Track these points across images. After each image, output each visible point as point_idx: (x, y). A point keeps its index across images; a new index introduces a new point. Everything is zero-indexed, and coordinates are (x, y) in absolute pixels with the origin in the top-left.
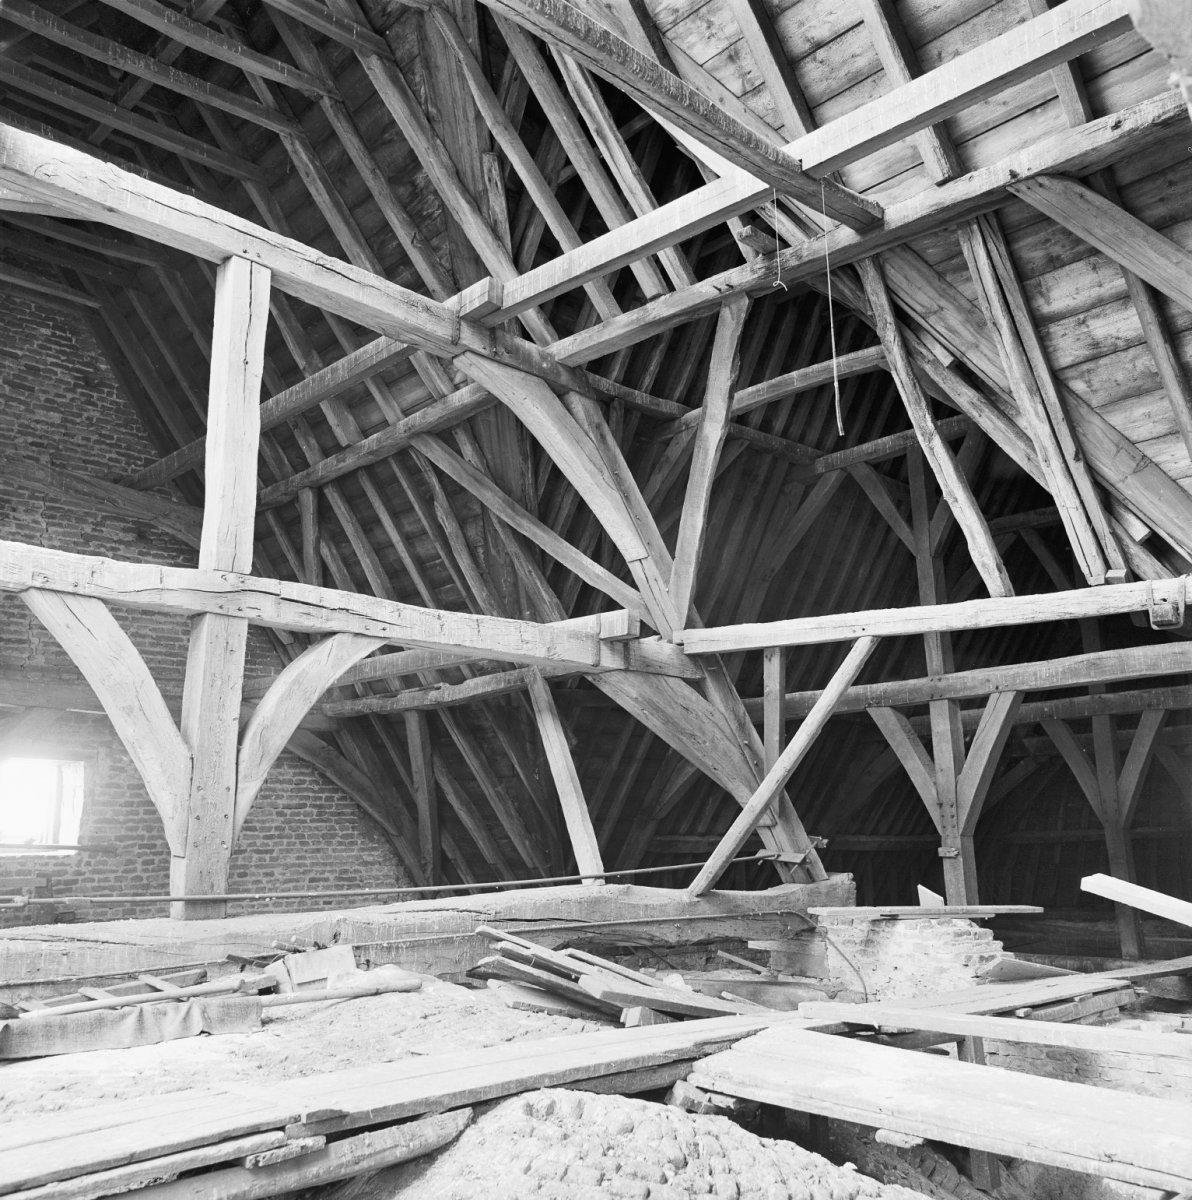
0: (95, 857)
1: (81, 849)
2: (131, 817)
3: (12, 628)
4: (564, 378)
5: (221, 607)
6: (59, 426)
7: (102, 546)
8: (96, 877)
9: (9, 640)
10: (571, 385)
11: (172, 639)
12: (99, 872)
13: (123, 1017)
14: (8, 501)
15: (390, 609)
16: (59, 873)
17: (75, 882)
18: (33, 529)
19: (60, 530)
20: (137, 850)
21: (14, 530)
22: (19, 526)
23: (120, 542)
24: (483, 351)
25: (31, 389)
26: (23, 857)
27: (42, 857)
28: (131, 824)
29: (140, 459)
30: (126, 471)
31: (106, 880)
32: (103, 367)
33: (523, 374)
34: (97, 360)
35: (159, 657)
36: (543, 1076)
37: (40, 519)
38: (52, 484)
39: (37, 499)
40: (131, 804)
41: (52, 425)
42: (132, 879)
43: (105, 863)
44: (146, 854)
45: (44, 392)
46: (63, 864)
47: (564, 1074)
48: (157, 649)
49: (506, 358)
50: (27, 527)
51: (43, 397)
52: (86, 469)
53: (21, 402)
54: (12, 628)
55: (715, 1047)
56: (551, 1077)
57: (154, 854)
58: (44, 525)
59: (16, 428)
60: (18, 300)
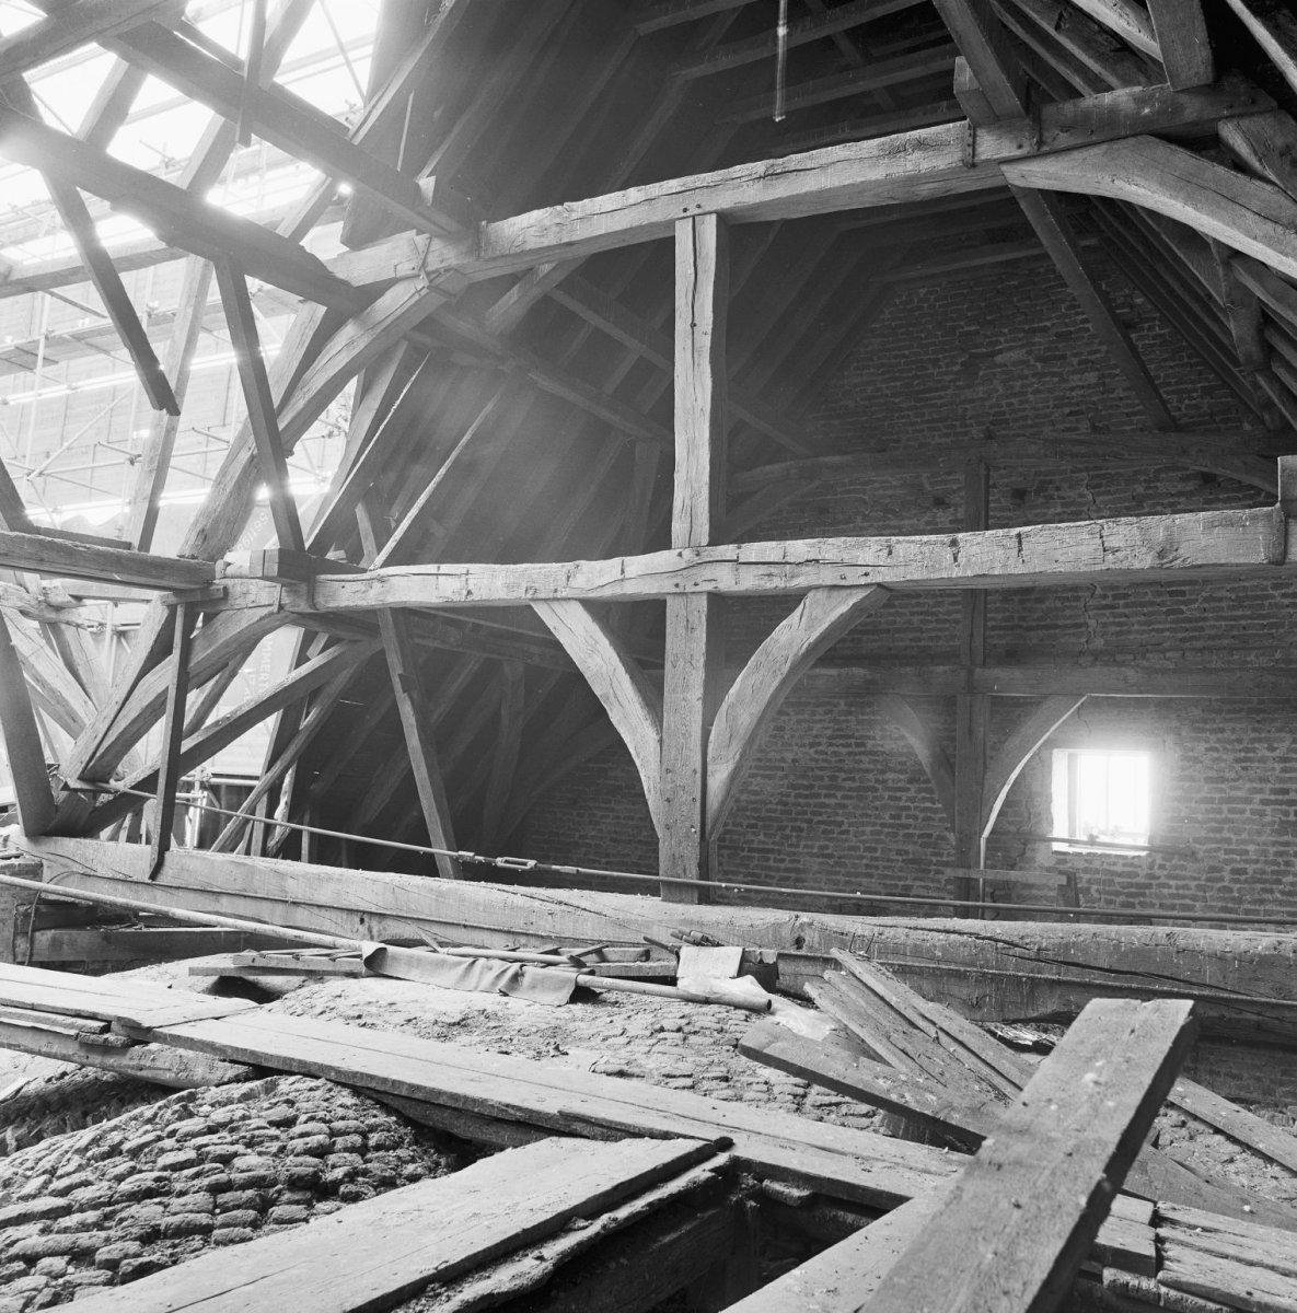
0: (1170, 860)
1: (1152, 850)
2: (1211, 816)
3: (1068, 612)
4: (1193, 110)
5: (677, 585)
6: (1097, 385)
7: (1158, 504)
8: (1172, 883)
9: (1066, 626)
10: (1209, 113)
11: (1257, 597)
12: (1176, 877)
13: (460, 963)
14: (1051, 482)
15: (875, 547)
16: (1129, 875)
17: (1149, 886)
18: (1080, 504)
19: (1107, 498)
20: (1221, 855)
21: (1059, 510)
22: (1064, 505)
23: (1180, 494)
24: (1018, 153)
25: (1064, 357)
26: (1089, 854)
27: (1109, 856)
28: (1214, 824)
29: (1195, 390)
30: (1180, 409)
31: (1186, 887)
32: (1139, 301)
33: (1132, 141)
34: (1131, 296)
35: (1243, 622)
36: (331, 1068)
37: (1086, 492)
38: (1046, 456)
39: (1080, 471)
40: (1211, 801)
41: (1089, 387)
42: (1219, 889)
43: (1183, 868)
44: (1236, 861)
45: (1075, 355)
46: (1132, 865)
47: (355, 1074)
48: (1240, 613)
49: (1064, 139)
50: (1072, 504)
51: (1075, 361)
52: (1131, 423)
53: (1054, 374)
54: (1068, 612)
55: (598, 1130)
56: (338, 1071)
57: (1246, 861)
58: (1090, 497)
59: (1051, 403)
60: (1042, 270)
